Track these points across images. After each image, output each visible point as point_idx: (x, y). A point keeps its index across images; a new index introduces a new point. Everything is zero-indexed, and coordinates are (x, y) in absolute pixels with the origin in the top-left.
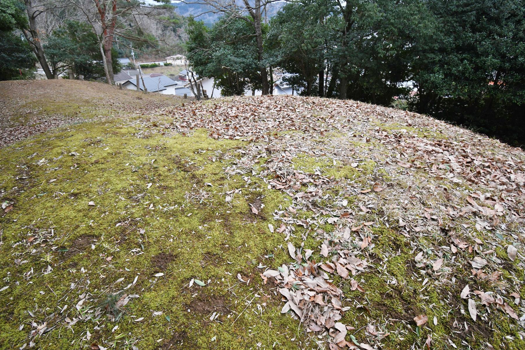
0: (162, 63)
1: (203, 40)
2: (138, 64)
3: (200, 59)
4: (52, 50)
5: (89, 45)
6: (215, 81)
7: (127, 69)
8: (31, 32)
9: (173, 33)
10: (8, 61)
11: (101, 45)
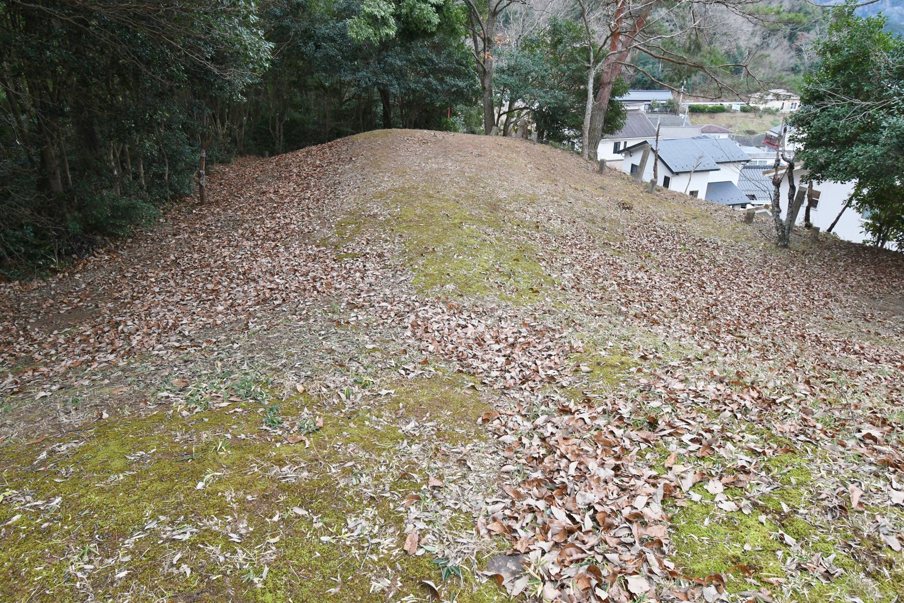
0: (736, 106)
1: (863, 73)
2: (686, 103)
3: (833, 129)
4: (506, 77)
5: (574, 71)
6: (859, 187)
7: (661, 112)
8: (484, 40)
9: (786, 42)
10: (436, 91)
11: (593, 73)
